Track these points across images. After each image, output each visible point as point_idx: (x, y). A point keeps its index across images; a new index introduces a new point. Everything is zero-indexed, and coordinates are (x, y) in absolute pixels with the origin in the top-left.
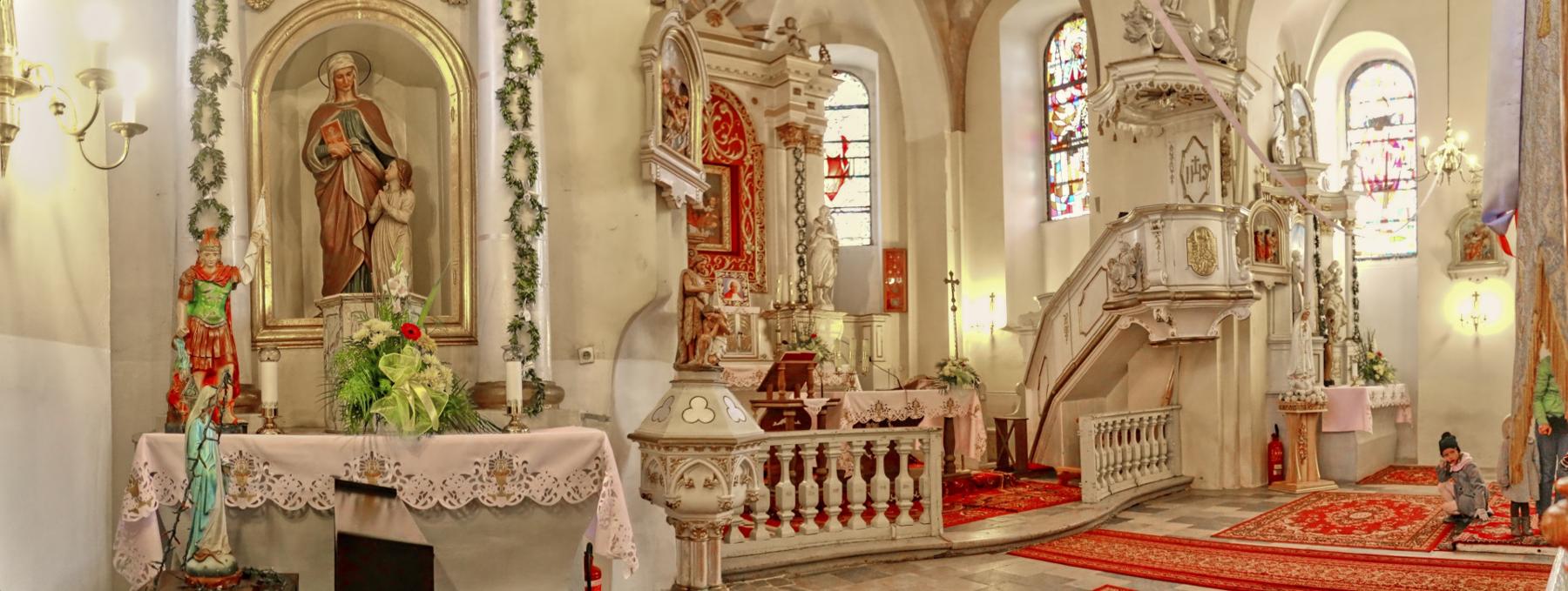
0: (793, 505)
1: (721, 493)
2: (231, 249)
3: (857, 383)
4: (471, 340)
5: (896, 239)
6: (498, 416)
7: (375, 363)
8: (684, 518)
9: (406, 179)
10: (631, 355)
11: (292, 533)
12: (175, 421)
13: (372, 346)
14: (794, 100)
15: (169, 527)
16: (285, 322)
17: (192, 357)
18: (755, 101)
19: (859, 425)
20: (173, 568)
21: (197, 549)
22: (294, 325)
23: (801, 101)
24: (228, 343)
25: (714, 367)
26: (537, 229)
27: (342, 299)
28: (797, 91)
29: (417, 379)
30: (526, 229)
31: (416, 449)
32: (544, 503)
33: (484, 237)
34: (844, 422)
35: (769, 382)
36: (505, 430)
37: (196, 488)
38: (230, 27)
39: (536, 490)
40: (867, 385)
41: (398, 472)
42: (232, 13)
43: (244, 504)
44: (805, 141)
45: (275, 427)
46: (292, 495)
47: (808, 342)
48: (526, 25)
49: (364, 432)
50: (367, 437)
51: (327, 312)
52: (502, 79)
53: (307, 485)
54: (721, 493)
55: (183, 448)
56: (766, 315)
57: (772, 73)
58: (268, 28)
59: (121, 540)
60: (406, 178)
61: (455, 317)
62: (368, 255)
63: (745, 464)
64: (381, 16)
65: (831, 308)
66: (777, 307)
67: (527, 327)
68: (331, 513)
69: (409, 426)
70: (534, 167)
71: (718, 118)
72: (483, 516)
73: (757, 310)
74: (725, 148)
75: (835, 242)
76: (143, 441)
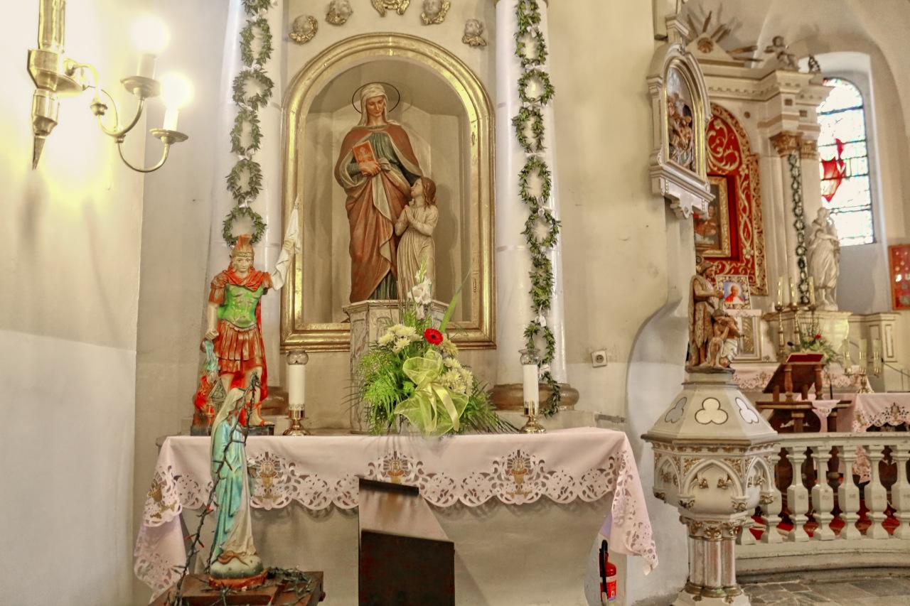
0: (806, 508)
1: (735, 494)
2: (264, 256)
3: (868, 386)
4: (489, 344)
6: (516, 417)
7: (398, 366)
8: (698, 518)
9: (431, 196)
10: (643, 358)
11: (317, 531)
12: (201, 423)
13: (396, 350)
14: (786, 110)
15: (193, 531)
16: (314, 327)
17: (220, 359)
18: (747, 115)
19: (873, 428)
20: (196, 571)
21: (222, 551)
22: (321, 331)
23: (794, 110)
24: (257, 346)
25: (725, 369)
26: (551, 240)
27: (368, 305)
28: (788, 102)
29: (442, 381)
30: (540, 240)
31: (437, 449)
32: (560, 501)
33: (501, 249)
34: (856, 425)
35: (776, 384)
36: (522, 431)
37: (220, 490)
38: (273, 54)
39: (552, 488)
40: (878, 388)
41: (420, 471)
42: (276, 42)
43: (270, 505)
44: (799, 147)
45: (301, 428)
46: (317, 494)
47: (813, 343)
48: (538, 62)
49: (388, 433)
50: (391, 438)
51: (354, 317)
52: (517, 109)
53: (332, 485)
54: (735, 494)
55: (208, 451)
56: (768, 318)
57: (763, 89)
58: (308, 59)
59: (142, 546)
60: (431, 196)
61: (474, 321)
62: (394, 264)
63: (759, 466)
64: (410, 54)
65: (835, 308)
66: (779, 309)
67: (542, 332)
68: (355, 511)
69: (431, 427)
70: (546, 186)
71: (713, 133)
72: (502, 514)
73: (758, 312)
74: (720, 160)
75: (835, 243)
76: (167, 444)
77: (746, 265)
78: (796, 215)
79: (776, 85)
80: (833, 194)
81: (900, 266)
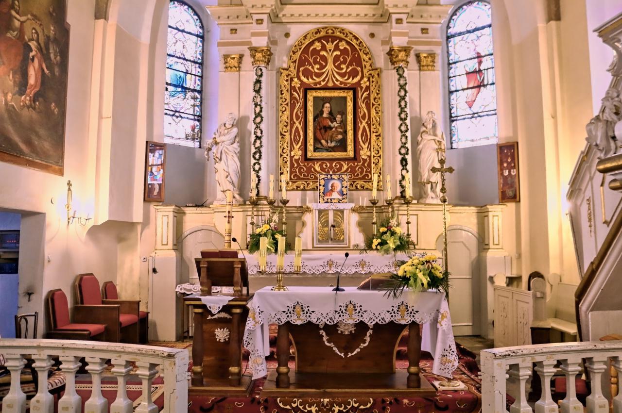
5: (511, 134)
18: (372, 35)
71: (338, 53)
77: (363, 164)
78: (401, 119)
79: (386, 7)
80: (474, 101)
81: (507, 162)
